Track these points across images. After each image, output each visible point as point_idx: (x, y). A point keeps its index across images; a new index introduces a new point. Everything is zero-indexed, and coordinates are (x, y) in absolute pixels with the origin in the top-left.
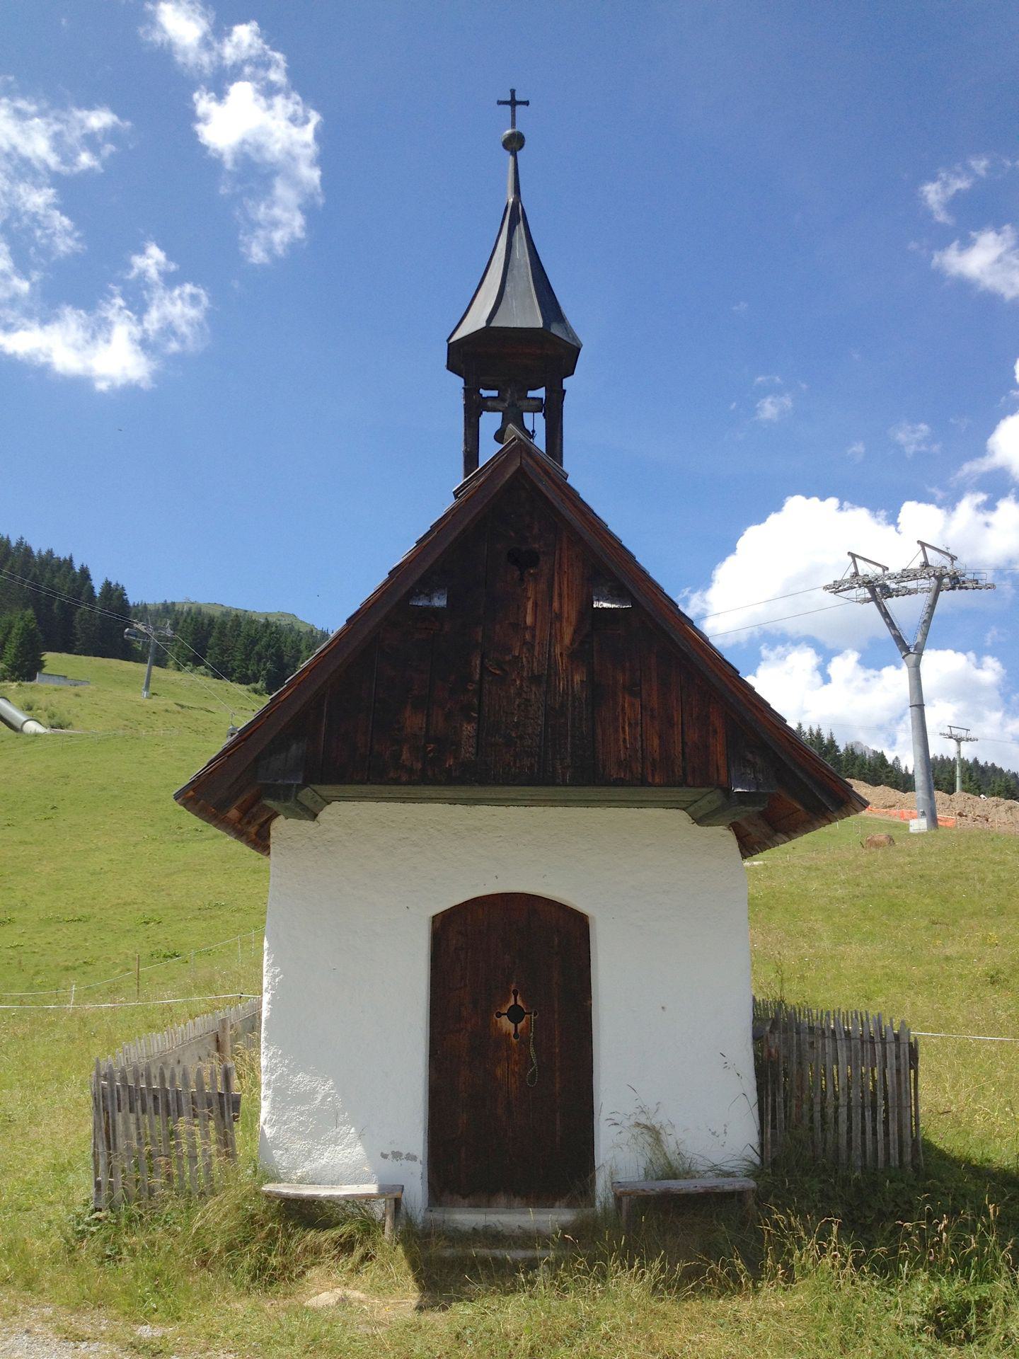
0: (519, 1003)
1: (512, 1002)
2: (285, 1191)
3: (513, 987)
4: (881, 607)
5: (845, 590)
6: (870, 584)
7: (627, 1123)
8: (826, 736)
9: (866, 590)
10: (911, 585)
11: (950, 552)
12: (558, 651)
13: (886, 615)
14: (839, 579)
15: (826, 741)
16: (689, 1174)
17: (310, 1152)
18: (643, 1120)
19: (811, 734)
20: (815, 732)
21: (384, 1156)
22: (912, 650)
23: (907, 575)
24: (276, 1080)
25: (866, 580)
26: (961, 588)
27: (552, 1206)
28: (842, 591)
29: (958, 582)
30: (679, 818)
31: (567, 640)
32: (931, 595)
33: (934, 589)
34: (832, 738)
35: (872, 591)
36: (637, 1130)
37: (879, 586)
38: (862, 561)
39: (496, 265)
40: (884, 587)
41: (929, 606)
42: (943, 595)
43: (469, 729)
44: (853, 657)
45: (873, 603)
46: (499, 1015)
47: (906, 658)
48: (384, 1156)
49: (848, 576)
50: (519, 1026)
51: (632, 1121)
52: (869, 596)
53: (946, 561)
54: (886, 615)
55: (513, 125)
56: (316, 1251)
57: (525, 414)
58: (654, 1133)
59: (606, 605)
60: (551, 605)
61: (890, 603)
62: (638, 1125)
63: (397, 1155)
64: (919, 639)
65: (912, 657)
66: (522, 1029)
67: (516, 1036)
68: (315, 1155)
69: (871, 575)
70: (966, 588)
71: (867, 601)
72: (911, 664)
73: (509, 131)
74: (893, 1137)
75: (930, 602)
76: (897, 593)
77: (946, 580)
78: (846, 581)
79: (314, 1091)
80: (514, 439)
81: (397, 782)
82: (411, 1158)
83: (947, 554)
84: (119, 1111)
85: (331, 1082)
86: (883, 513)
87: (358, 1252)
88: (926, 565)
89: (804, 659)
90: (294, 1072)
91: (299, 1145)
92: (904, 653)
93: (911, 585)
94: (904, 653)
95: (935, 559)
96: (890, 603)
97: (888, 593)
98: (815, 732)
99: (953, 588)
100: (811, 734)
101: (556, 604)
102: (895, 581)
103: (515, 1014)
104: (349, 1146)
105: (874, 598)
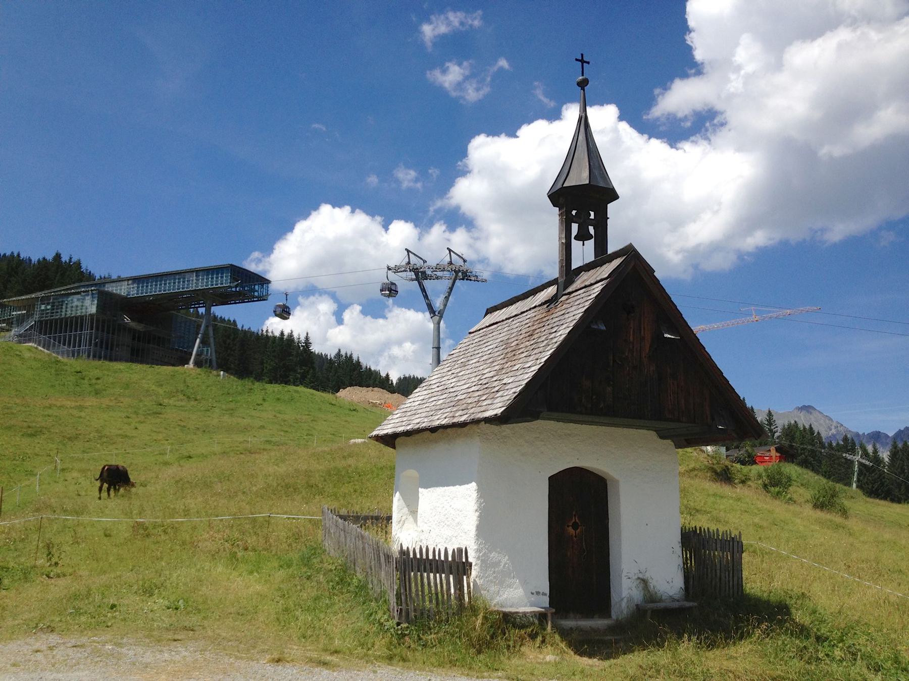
0: (577, 521)
1: (574, 521)
2: (504, 610)
3: (574, 513)
4: (420, 284)
5: (401, 271)
6: (416, 271)
7: (634, 578)
8: (355, 358)
9: (413, 273)
10: (439, 274)
11: (464, 257)
12: (644, 355)
13: (423, 290)
14: (398, 264)
15: (354, 361)
16: (660, 600)
17: (499, 591)
18: (641, 576)
19: (346, 356)
20: (348, 356)
21: (532, 594)
22: (437, 313)
23: (439, 268)
24: (482, 556)
25: (415, 268)
26: (467, 279)
27: (593, 618)
28: (399, 272)
29: (467, 276)
30: (652, 435)
31: (647, 351)
32: (451, 281)
33: (453, 277)
34: (358, 360)
35: (417, 274)
36: (639, 581)
37: (421, 272)
38: (413, 255)
39: (580, 148)
40: (424, 273)
41: (450, 288)
42: (458, 283)
43: (609, 389)
44: (358, 308)
45: (416, 282)
46: (568, 526)
47: (433, 318)
48: (532, 594)
49: (404, 263)
50: (577, 531)
51: (636, 577)
52: (414, 277)
53: (461, 262)
54: (423, 290)
55: (583, 75)
56: (522, 638)
57: (573, 224)
58: (644, 582)
59: (669, 336)
60: (640, 332)
61: (426, 283)
62: (639, 578)
63: (538, 593)
64: (442, 307)
65: (437, 318)
66: (578, 534)
67: (576, 537)
68: (501, 593)
69: (418, 266)
70: (471, 280)
71: (412, 280)
72: (436, 322)
73: (581, 78)
74: (735, 583)
75: (450, 286)
76: (431, 278)
77: (460, 274)
78: (402, 266)
79: (500, 561)
80: (632, 252)
81: (581, 413)
82: (544, 594)
83: (462, 258)
84: (412, 571)
85: (507, 557)
86: (378, 219)
87: (539, 638)
88: (451, 263)
89: (325, 307)
90: (490, 552)
91: (493, 588)
92: (432, 315)
93: (439, 274)
94: (432, 315)
95: (458, 262)
96: (426, 283)
97: (425, 276)
98: (348, 356)
99: (463, 279)
100: (346, 356)
101: (642, 333)
102: (432, 270)
103: (575, 526)
104: (516, 589)
105: (417, 279)
